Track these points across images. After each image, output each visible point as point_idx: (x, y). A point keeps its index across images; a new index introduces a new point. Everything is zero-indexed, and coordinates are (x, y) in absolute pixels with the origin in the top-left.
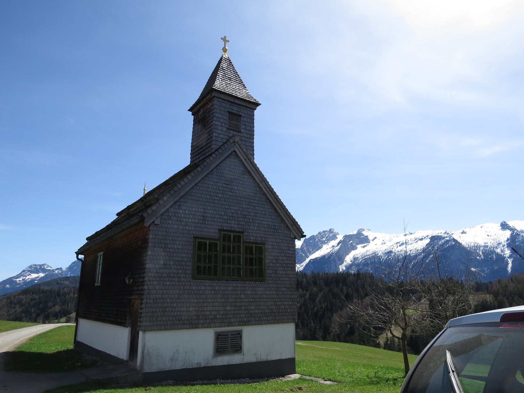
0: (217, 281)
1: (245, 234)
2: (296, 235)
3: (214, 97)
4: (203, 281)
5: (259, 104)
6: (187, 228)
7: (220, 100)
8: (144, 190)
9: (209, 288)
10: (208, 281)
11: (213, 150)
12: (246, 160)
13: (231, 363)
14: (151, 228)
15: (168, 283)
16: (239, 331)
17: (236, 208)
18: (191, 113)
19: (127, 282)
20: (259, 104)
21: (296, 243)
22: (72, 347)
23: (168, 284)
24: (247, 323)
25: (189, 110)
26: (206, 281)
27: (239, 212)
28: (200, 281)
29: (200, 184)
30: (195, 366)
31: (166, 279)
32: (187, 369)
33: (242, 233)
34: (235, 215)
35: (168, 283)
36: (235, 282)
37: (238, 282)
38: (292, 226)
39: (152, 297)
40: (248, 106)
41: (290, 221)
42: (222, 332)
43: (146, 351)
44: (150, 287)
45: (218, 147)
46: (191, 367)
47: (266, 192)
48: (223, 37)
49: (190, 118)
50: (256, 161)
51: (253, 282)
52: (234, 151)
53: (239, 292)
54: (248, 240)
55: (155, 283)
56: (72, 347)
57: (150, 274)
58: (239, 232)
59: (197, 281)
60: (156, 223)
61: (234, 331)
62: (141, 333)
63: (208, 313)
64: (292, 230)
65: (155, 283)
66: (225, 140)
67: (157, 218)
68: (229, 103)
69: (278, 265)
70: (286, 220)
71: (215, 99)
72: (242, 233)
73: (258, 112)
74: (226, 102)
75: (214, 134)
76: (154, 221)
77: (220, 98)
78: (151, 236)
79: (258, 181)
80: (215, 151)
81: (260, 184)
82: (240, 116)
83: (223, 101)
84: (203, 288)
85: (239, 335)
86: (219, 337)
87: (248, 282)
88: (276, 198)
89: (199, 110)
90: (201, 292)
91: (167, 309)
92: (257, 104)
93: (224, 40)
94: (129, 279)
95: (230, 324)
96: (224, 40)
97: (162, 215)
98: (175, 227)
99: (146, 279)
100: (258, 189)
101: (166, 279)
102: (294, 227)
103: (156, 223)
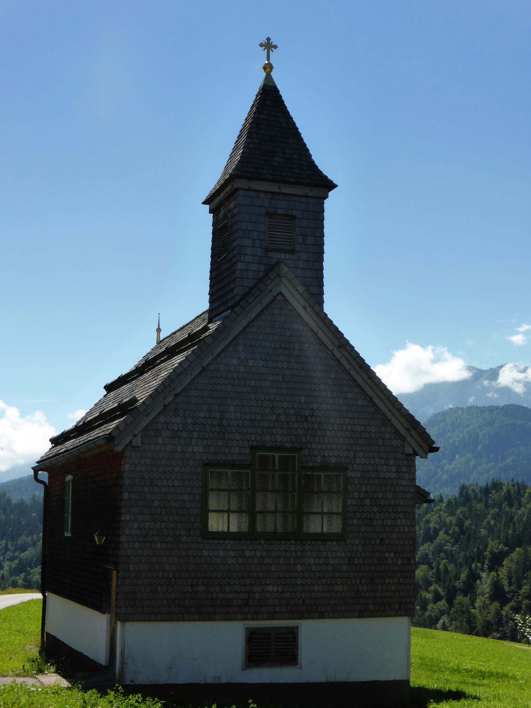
0: (248, 542)
1: (306, 452)
2: (417, 448)
3: (237, 190)
4: (221, 542)
5: (335, 186)
6: (190, 449)
7: (250, 193)
8: (159, 330)
9: (232, 553)
10: (232, 542)
11: (238, 298)
12: (304, 308)
13: (275, 681)
14: (127, 453)
15: (159, 546)
16: (292, 628)
17: (285, 405)
18: (207, 207)
19: (97, 543)
20: (335, 186)
21: (417, 462)
22: (520, 390)
23: (159, 548)
24: (302, 617)
25: (205, 203)
26: (227, 541)
27: (292, 412)
28: (215, 542)
29: (212, 367)
30: (210, 680)
31: (156, 539)
32: (197, 684)
33: (299, 450)
34: (283, 418)
35: (159, 546)
36: (283, 542)
37: (288, 543)
38: (408, 430)
39: (132, 568)
40: (310, 194)
41: (402, 419)
42: (259, 629)
43: (126, 652)
44: (129, 553)
45: (247, 289)
46: (203, 682)
47: (347, 366)
48: (263, 40)
49: (205, 220)
50: (325, 310)
51: (319, 543)
52: (281, 293)
53: (292, 561)
54: (311, 464)
55: (137, 545)
56: (520, 390)
57: (127, 531)
58: (292, 449)
59: (210, 541)
60: (134, 444)
61: (281, 628)
62: (119, 623)
63: (231, 596)
64: (409, 439)
65: (137, 545)
66: (262, 274)
67: (135, 436)
68: (269, 196)
69: (375, 509)
70: (394, 421)
71: (240, 193)
72: (299, 450)
73: (333, 206)
74: (262, 195)
75: (239, 266)
76: (131, 442)
77: (249, 189)
78: (127, 467)
79: (331, 348)
80: (241, 300)
81: (336, 352)
82: (294, 218)
83: (255, 194)
84: (221, 553)
85: (292, 635)
86: (253, 637)
87: (309, 543)
88: (370, 378)
89: (220, 204)
90: (219, 560)
91: (159, 589)
92: (331, 186)
93: (268, 46)
94: (100, 535)
95: (272, 616)
96: (268, 46)
97: (145, 429)
98: (169, 448)
99: (123, 539)
100: (333, 363)
101: (156, 539)
102: (413, 432)
103: (134, 444)
